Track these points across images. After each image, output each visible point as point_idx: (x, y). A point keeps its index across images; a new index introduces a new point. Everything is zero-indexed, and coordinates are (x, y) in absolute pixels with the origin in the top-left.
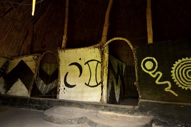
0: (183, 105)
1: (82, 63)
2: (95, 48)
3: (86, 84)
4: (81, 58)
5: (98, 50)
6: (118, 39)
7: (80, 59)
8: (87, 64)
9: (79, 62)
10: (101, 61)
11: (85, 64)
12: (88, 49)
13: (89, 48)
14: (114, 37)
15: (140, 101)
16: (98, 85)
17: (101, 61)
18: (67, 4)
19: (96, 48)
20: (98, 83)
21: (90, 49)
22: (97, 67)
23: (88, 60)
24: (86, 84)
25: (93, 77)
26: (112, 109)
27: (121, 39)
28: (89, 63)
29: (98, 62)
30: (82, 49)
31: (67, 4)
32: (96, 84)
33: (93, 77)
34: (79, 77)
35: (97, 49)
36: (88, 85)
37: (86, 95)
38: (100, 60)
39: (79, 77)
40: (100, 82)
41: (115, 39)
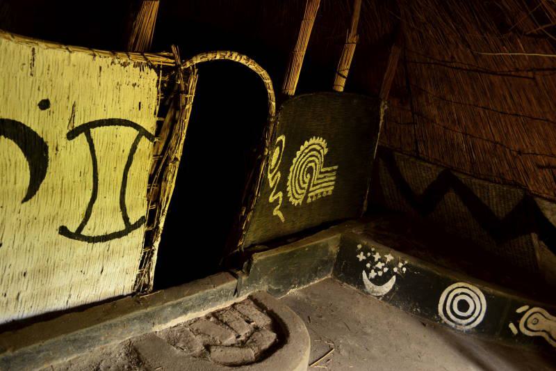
0: (307, 247)
1: (50, 128)
2: (147, 69)
3: (63, 231)
4: (52, 101)
5: (156, 78)
6: (243, 61)
7: (44, 105)
8: (82, 136)
9: (33, 120)
10: (153, 133)
11: (72, 135)
12: (113, 63)
13: (116, 61)
14: (232, 49)
15: (255, 262)
16: (130, 228)
17: (153, 133)
18: (358, 7)
19: (152, 67)
20: (132, 221)
21: (125, 65)
22: (135, 156)
23: (92, 119)
24: (63, 231)
25: (108, 199)
26: (192, 306)
27: (253, 66)
28: (96, 132)
29: (143, 132)
30: (81, 56)
31: (358, 7)
32: (121, 226)
33: (108, 199)
34: (25, 200)
35: (153, 74)
36: (77, 235)
37: (60, 280)
38: (149, 124)
39: (25, 200)
40: (143, 217)
41: (236, 57)
